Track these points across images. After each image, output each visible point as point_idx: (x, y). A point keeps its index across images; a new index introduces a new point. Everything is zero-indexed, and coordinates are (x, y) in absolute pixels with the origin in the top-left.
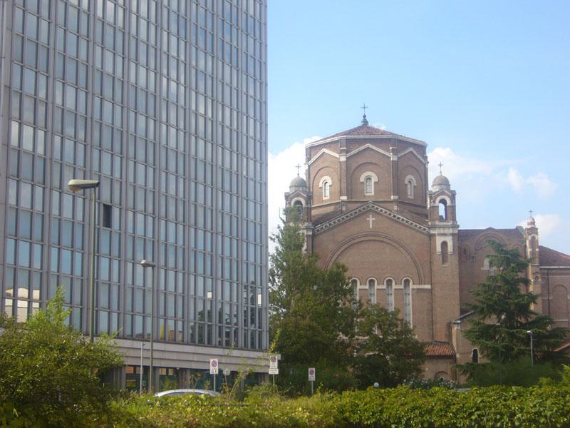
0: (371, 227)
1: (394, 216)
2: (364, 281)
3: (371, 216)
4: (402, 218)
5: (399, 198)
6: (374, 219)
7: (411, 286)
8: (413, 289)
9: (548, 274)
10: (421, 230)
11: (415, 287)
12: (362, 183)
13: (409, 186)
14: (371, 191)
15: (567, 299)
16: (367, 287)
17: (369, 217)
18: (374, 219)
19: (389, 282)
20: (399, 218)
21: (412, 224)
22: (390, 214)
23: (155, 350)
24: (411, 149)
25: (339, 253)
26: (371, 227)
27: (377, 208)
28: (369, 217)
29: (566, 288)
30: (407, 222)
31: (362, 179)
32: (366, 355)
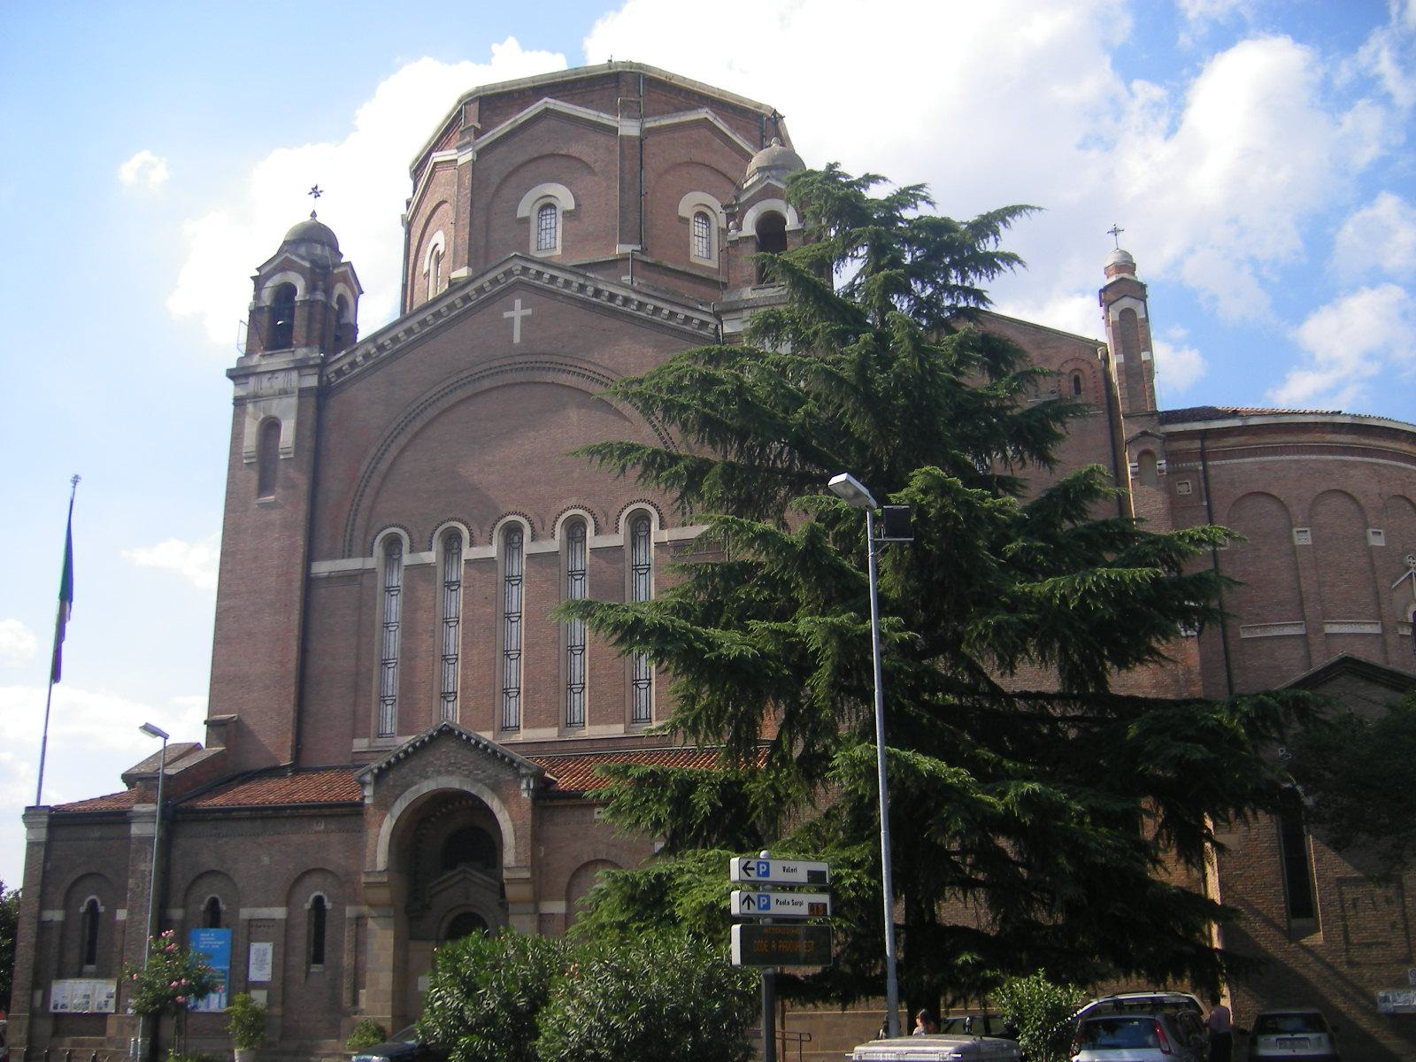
0: (517, 339)
1: (598, 293)
2: (612, 519)
3: (518, 303)
4: (622, 292)
5: (642, 252)
6: (529, 312)
7: (657, 534)
8: (659, 545)
9: (1203, 456)
10: (543, 282)
11: (666, 536)
12: (526, 220)
13: (698, 228)
14: (550, 241)
15: (1294, 547)
16: (374, 562)
17: (512, 308)
18: (529, 312)
19: (575, 529)
20: (612, 297)
21: (657, 310)
22: (582, 288)
23: (298, 751)
24: (704, 113)
25: (403, 440)
26: (517, 339)
27: (539, 274)
28: (512, 308)
29: (1282, 504)
30: (641, 306)
31: (525, 208)
32: (905, 668)
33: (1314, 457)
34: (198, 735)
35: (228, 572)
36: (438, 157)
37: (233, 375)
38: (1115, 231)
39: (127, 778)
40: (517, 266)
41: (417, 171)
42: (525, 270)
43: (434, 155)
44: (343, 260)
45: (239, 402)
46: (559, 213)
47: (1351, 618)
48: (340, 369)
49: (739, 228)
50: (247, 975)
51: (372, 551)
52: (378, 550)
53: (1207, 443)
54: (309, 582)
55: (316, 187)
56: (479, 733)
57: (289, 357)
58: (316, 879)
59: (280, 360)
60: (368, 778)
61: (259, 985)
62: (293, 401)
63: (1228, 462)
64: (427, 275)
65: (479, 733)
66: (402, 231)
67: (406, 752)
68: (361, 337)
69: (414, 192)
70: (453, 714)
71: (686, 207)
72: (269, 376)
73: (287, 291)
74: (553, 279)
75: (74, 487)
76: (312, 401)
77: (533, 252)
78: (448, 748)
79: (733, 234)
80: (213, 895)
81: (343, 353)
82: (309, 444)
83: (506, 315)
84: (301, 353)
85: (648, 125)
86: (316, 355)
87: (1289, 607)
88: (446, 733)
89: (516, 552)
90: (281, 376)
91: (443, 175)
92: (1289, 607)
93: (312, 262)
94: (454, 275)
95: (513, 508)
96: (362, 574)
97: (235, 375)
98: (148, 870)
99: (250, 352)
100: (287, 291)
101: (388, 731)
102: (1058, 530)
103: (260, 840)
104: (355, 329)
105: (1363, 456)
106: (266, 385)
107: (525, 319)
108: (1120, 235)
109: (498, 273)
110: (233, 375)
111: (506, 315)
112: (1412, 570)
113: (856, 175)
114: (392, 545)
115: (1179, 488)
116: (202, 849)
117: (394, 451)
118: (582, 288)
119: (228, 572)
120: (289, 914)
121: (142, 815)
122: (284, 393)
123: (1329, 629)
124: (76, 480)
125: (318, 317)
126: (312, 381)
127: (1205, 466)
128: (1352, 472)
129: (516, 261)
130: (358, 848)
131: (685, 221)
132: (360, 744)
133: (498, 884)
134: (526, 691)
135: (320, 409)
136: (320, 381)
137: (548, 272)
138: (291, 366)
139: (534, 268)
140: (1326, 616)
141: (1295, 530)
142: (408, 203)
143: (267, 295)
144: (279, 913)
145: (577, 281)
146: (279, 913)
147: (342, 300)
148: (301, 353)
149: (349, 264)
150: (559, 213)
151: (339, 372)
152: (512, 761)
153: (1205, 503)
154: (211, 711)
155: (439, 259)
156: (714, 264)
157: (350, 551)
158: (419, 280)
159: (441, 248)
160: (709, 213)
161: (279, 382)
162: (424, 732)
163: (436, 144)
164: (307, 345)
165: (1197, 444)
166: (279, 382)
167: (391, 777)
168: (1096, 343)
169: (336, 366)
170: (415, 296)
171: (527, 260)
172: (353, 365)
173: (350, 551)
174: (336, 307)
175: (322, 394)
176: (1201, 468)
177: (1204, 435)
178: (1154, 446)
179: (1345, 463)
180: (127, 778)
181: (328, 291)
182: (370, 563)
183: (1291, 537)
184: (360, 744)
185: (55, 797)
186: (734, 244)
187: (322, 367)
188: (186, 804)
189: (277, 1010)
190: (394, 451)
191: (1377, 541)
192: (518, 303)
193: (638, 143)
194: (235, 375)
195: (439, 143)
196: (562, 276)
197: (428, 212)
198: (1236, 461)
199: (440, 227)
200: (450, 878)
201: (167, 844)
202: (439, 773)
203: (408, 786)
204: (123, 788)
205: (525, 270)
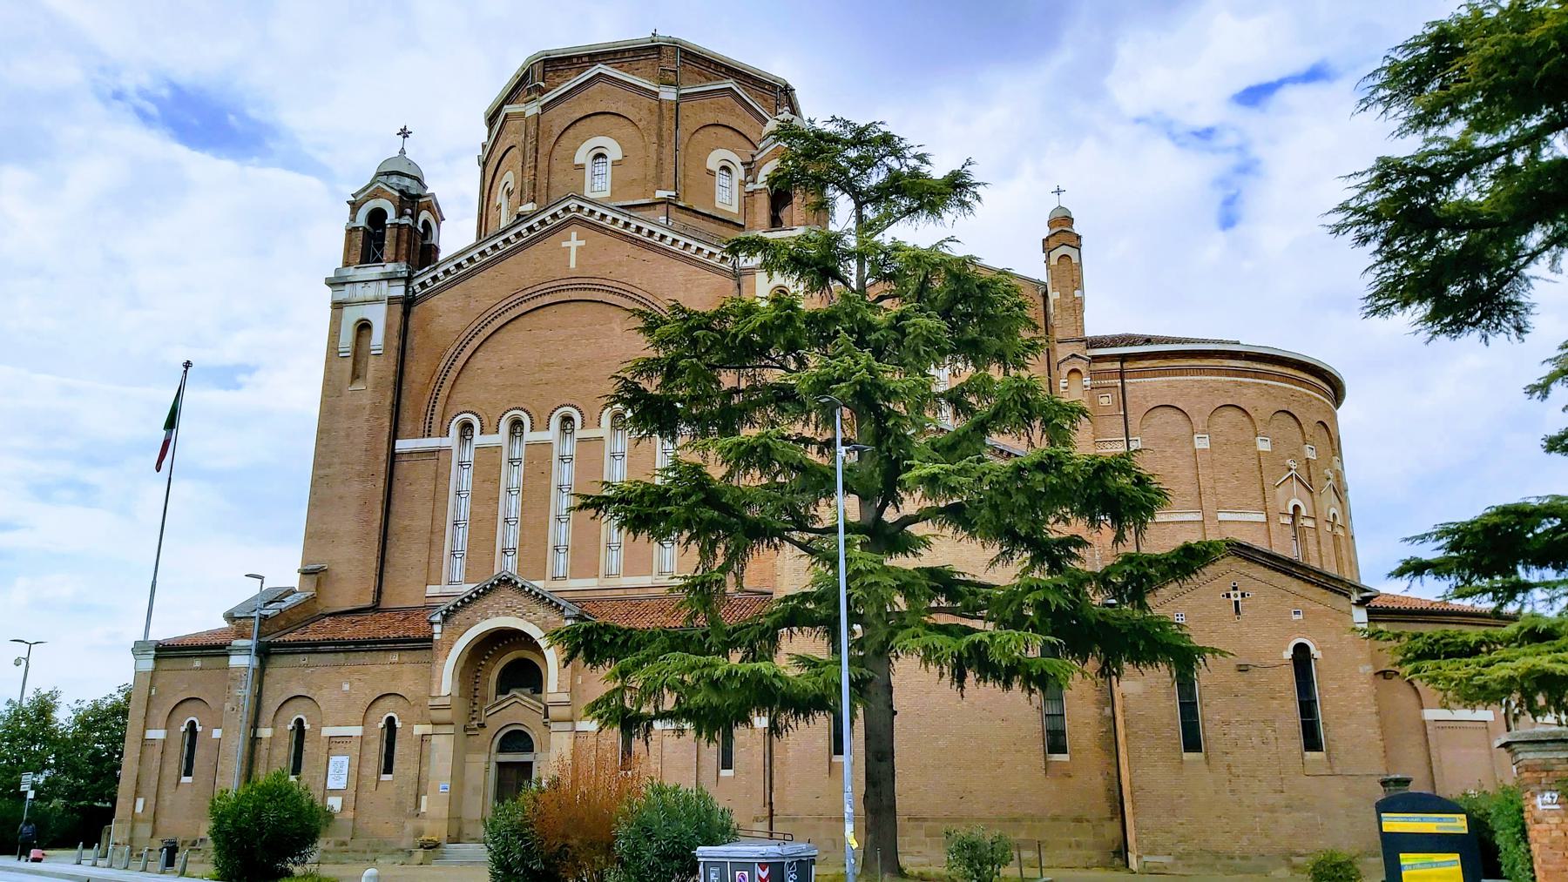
0: (573, 264)
3: (574, 235)
5: (677, 196)
6: (582, 243)
9: (1122, 375)
12: (581, 167)
13: (721, 179)
18: (582, 243)
20: (651, 233)
24: (729, 83)
26: (573, 264)
31: (583, 156)
33: (1213, 378)
34: (293, 580)
35: (325, 446)
36: (508, 109)
37: (331, 283)
38: (1058, 192)
39: (230, 617)
40: (573, 204)
41: (491, 120)
42: (580, 208)
43: (505, 107)
44: (428, 192)
45: (338, 306)
46: (609, 161)
47: (1240, 508)
48: (424, 282)
49: (754, 181)
50: (326, 785)
51: (448, 432)
52: (454, 431)
53: (1125, 365)
54: (393, 456)
55: (405, 129)
56: (533, 583)
57: (380, 270)
58: (388, 702)
59: (374, 271)
60: (438, 618)
61: (335, 792)
62: (383, 308)
63: (1142, 380)
64: (499, 207)
65: (533, 583)
66: (479, 169)
67: (470, 597)
68: (441, 257)
69: (489, 137)
70: (509, 565)
71: (713, 162)
72: (363, 284)
73: (377, 216)
74: (603, 216)
75: (186, 372)
76: (399, 308)
77: (588, 194)
78: (506, 594)
79: (750, 187)
80: (299, 716)
81: (427, 268)
82: (396, 343)
83: (564, 244)
84: (390, 267)
85: (683, 92)
86: (402, 268)
87: (1189, 498)
88: (506, 582)
89: (568, 436)
90: (373, 285)
91: (511, 125)
92: (1189, 498)
93: (401, 191)
94: (521, 209)
95: (567, 402)
96: (439, 451)
97: (335, 283)
98: (242, 695)
99: (347, 264)
100: (377, 216)
101: (457, 580)
102: (1464, 191)
103: (343, 670)
104: (437, 250)
105: (1256, 377)
106: (361, 292)
107: (579, 249)
108: (1062, 194)
109: (558, 209)
110: (331, 283)
111: (564, 244)
112: (1293, 472)
113: (863, 126)
114: (466, 427)
115: (1101, 400)
116: (287, 676)
117: (468, 351)
118: (627, 225)
119: (325, 446)
120: (364, 731)
121: (240, 650)
122: (377, 301)
123: (1221, 517)
124: (188, 365)
125: (405, 237)
126: (399, 290)
127: (1123, 382)
128: (1245, 391)
129: (573, 201)
130: (430, 679)
131: (711, 173)
132: (432, 590)
133: (543, 707)
134: (573, 547)
135: (406, 314)
136: (407, 291)
137: (599, 211)
138: (382, 277)
139: (587, 207)
140: (1220, 507)
141: (1196, 436)
142: (484, 146)
143: (361, 221)
144: (357, 731)
145: (622, 220)
146: (357, 731)
147: (426, 224)
148: (390, 267)
149: (433, 195)
150: (609, 164)
151: (423, 285)
152: (558, 605)
153: (1122, 413)
154: (305, 561)
155: (509, 193)
156: (735, 209)
157: (429, 431)
158: (492, 213)
159: (511, 186)
160: (731, 166)
161: (370, 292)
162: (487, 580)
163: (508, 97)
164: (396, 261)
165: (1117, 365)
166: (370, 292)
167: (458, 618)
168: (1039, 282)
169: (421, 280)
170: (489, 224)
171: (583, 200)
172: (435, 279)
173: (429, 431)
174: (422, 230)
175: (408, 303)
176: (1120, 384)
177: (1123, 358)
178: (1082, 366)
179: (1239, 384)
180: (230, 617)
181: (415, 217)
182: (444, 442)
183: (1192, 441)
184: (432, 590)
185: (160, 634)
186: (753, 193)
187: (408, 280)
188: (281, 639)
189: (350, 814)
190: (468, 351)
191: (1264, 446)
192: (574, 235)
193: (674, 107)
194: (335, 283)
195: (510, 96)
196: (611, 215)
197: (501, 155)
198: (1149, 380)
199: (510, 168)
200: (503, 701)
201: (261, 673)
202: (497, 615)
203: (471, 626)
204: (225, 624)
205: (580, 208)
